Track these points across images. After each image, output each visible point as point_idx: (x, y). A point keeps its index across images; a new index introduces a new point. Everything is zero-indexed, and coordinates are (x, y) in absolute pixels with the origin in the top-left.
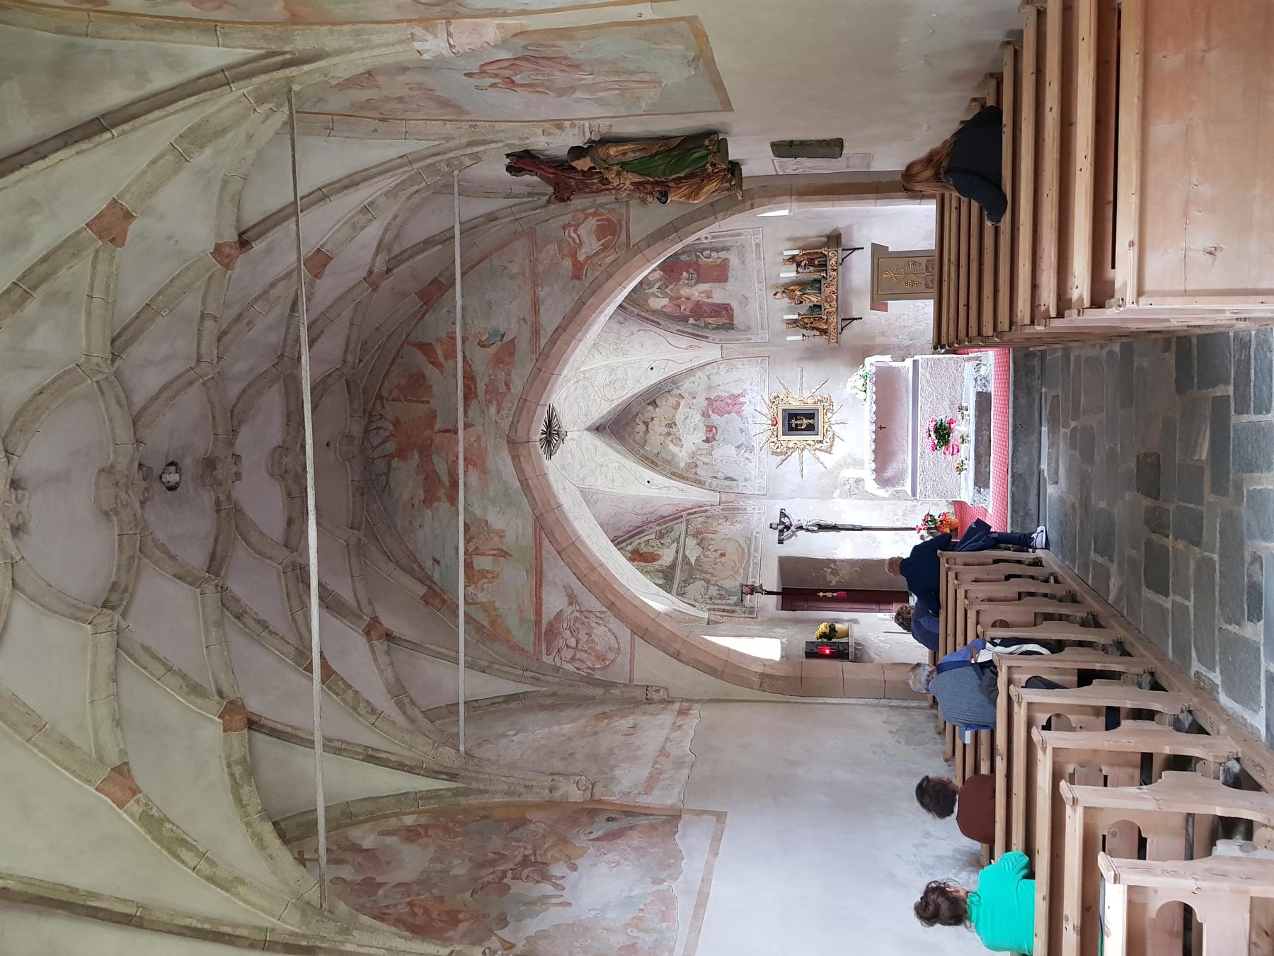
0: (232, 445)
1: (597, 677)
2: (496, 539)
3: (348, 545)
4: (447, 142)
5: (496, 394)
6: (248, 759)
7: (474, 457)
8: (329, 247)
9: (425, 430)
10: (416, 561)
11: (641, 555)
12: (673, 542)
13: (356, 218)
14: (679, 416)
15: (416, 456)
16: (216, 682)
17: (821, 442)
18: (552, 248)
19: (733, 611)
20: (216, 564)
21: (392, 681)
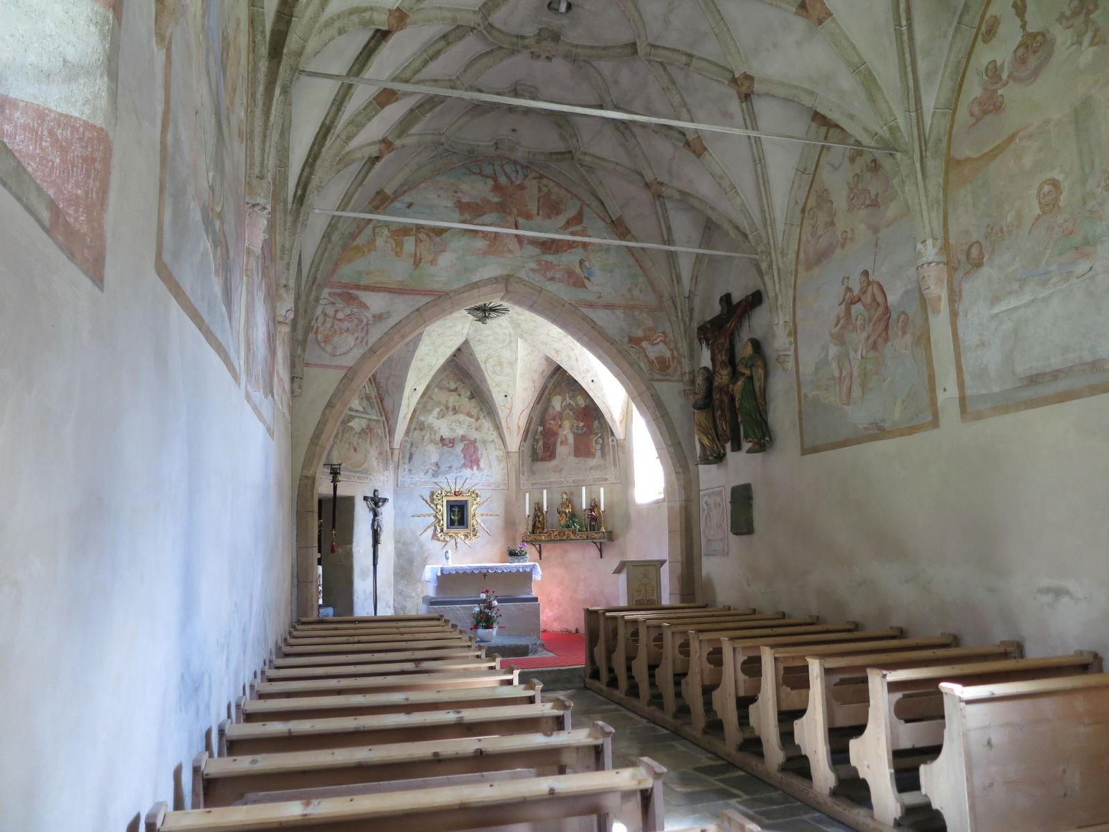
0: (566, 57)
1: (310, 335)
2: (430, 258)
3: (440, 134)
4: (780, 253)
7: (495, 246)
8: (708, 157)
9: (517, 209)
10: (410, 189)
12: (364, 408)
14: (462, 417)
15: (496, 200)
17: (442, 531)
18: (649, 323)
21: (353, 157)
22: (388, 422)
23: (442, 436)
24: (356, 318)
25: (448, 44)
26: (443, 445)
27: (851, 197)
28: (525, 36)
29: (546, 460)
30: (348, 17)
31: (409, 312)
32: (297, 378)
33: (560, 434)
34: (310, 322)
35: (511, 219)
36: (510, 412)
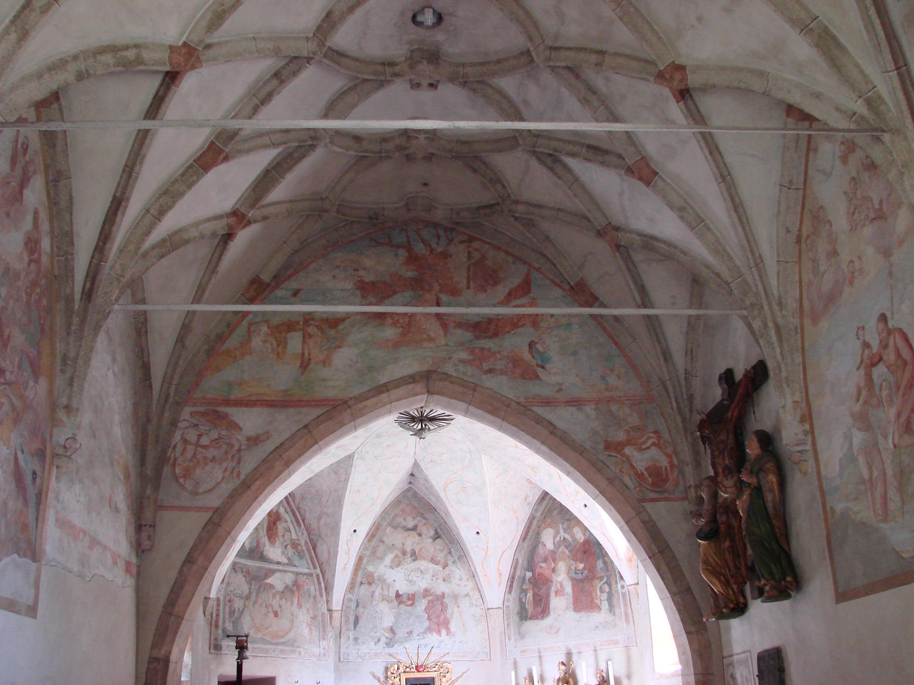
0: (452, 80)
2: (322, 357)
5: (480, 357)
6: (142, 68)
7: (411, 334)
8: (660, 184)
9: (440, 284)
10: (296, 272)
11: (275, 523)
12: (289, 559)
13: (690, 211)
14: (423, 564)
15: (410, 274)
16: (219, 44)
18: (634, 420)
19: (217, 626)
20: (337, 56)
21: (186, 236)
22: (323, 576)
23: (397, 591)
24: (225, 443)
25: (282, 82)
26: (400, 603)
27: (852, 211)
28: (394, 62)
29: (537, 618)
30: (95, 58)
31: (294, 430)
32: (145, 526)
33: (554, 580)
34: (164, 452)
35: (430, 297)
36: (486, 554)
